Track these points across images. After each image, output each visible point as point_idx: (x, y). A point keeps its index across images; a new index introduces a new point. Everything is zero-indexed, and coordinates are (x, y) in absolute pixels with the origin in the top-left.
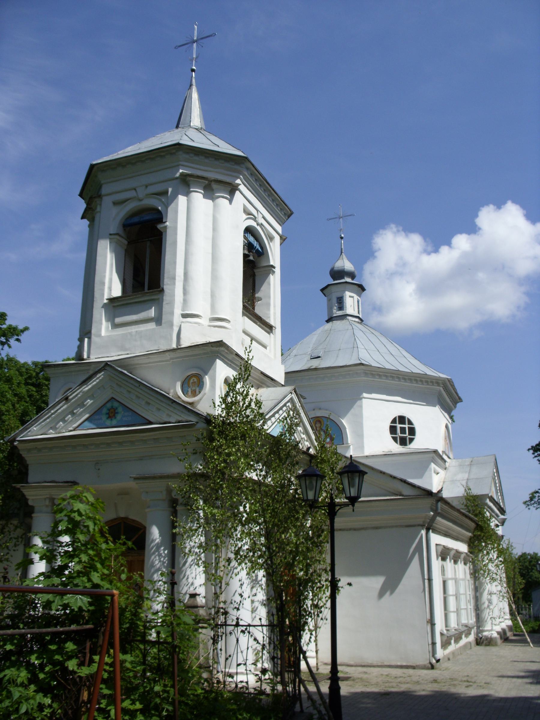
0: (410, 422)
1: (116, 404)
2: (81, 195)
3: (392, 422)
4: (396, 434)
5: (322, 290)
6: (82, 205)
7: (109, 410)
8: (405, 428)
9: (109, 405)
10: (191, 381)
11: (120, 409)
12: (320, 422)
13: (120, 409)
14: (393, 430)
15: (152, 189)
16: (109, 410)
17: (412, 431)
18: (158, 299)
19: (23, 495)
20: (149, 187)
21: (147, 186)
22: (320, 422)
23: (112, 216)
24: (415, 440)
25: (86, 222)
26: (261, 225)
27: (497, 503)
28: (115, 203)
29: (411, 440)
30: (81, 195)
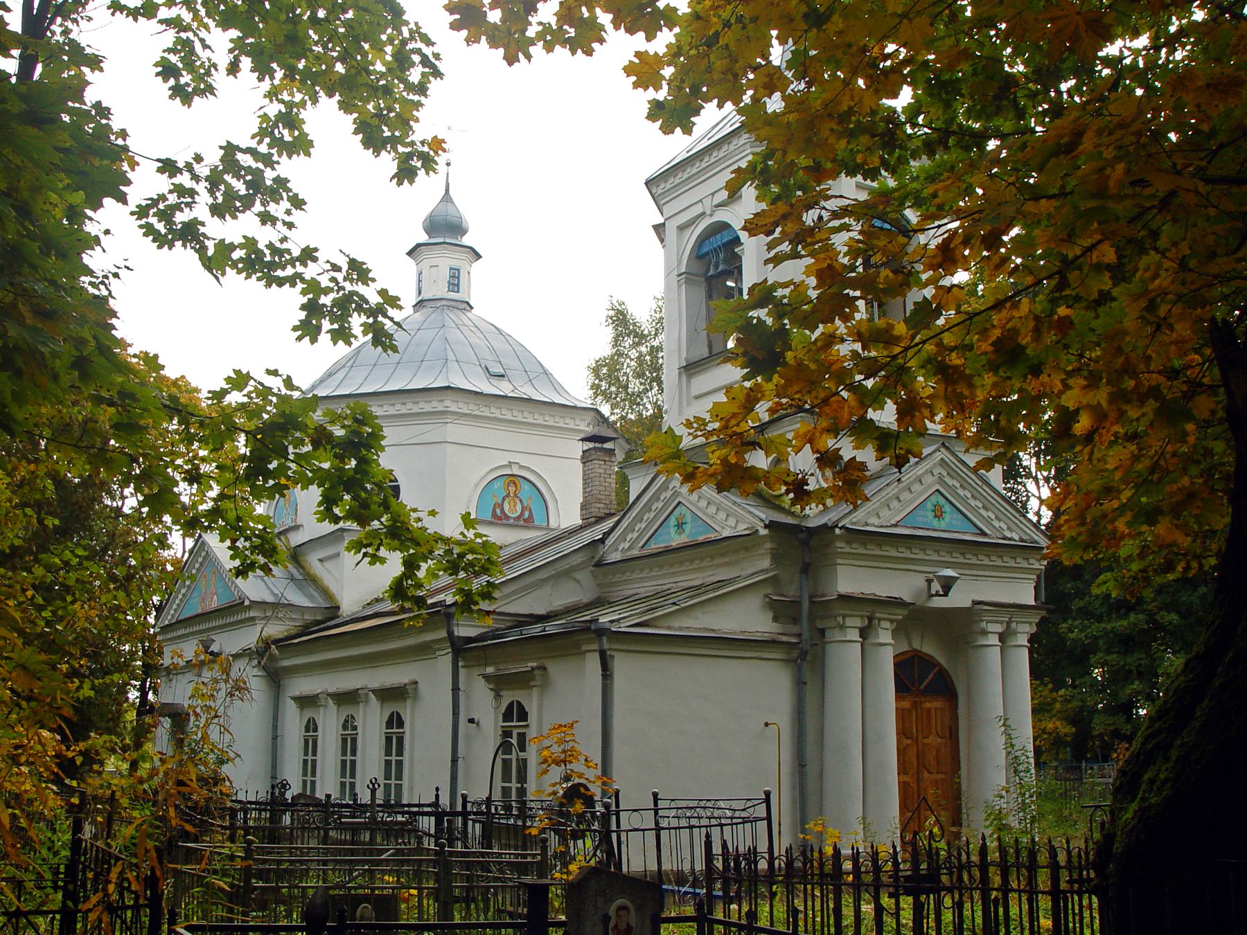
5: (410, 253)
12: (515, 483)
22: (515, 483)
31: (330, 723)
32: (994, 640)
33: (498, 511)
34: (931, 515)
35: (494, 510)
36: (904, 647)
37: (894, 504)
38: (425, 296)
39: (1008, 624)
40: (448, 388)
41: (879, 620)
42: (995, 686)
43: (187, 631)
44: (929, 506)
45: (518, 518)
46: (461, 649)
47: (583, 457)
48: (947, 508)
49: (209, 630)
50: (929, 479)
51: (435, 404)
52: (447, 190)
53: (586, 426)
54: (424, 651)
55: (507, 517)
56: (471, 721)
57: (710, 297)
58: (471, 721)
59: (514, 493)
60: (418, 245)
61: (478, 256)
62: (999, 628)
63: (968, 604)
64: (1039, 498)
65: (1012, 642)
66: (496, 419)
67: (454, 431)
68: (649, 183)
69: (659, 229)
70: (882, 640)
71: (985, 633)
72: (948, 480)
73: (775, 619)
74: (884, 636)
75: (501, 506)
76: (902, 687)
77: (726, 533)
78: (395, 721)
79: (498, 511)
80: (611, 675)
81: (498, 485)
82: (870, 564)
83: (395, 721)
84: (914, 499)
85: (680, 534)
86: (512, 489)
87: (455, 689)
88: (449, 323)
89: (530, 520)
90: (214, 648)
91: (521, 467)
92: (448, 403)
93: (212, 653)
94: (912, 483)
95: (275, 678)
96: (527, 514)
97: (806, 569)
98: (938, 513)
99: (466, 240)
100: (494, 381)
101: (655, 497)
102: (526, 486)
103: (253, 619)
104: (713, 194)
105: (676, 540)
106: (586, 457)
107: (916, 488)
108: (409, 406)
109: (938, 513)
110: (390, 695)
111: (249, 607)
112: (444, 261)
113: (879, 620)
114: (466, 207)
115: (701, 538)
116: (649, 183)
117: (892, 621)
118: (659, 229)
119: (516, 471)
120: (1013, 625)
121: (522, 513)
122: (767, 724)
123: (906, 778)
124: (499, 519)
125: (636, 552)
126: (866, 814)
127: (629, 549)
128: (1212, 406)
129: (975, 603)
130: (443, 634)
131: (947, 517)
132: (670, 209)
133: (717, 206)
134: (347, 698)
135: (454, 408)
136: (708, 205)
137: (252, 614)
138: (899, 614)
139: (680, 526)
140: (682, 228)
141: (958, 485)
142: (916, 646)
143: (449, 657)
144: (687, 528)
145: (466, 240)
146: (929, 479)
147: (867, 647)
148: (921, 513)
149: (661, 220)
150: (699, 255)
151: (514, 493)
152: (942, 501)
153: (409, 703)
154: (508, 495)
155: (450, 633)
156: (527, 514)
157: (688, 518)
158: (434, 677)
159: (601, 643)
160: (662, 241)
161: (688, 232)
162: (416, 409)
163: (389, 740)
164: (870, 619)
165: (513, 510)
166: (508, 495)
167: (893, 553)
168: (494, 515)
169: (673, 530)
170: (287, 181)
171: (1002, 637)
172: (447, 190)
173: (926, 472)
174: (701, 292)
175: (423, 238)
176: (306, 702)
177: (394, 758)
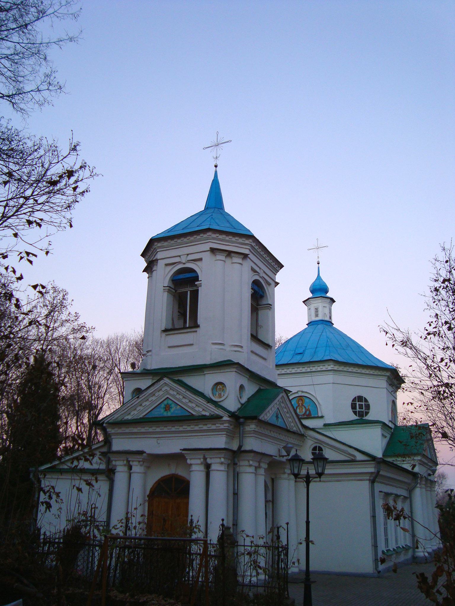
0: (366, 401)
1: (170, 402)
2: (143, 255)
3: (353, 401)
4: (356, 409)
5: (304, 302)
6: (144, 264)
7: (166, 406)
8: (362, 405)
9: (165, 402)
10: (218, 387)
11: (173, 405)
12: (302, 400)
13: (173, 405)
14: (353, 406)
15: (191, 257)
16: (166, 406)
17: (368, 407)
18: (196, 331)
19: (218, 541)
20: (189, 256)
21: (188, 255)
22: (302, 400)
23: (164, 274)
24: (370, 414)
25: (146, 275)
26: (263, 278)
27: (431, 459)
28: (167, 265)
29: (367, 413)
30: (143, 255)
44: (163, 405)
45: (304, 415)
52: (319, 274)
61: (334, 301)
82: (205, 434)
86: (300, 402)
87: (266, 506)
91: (302, 392)
96: (308, 412)
99: (328, 295)
102: (307, 400)
108: (327, 367)
109: (168, 408)
114: (325, 279)
119: (300, 394)
121: (306, 412)
128: (443, 356)
138: (268, 460)
145: (328, 295)
150: (262, 297)
152: (170, 402)
154: (299, 405)
156: (308, 412)
166: (299, 405)
172: (319, 274)
175: (310, 295)
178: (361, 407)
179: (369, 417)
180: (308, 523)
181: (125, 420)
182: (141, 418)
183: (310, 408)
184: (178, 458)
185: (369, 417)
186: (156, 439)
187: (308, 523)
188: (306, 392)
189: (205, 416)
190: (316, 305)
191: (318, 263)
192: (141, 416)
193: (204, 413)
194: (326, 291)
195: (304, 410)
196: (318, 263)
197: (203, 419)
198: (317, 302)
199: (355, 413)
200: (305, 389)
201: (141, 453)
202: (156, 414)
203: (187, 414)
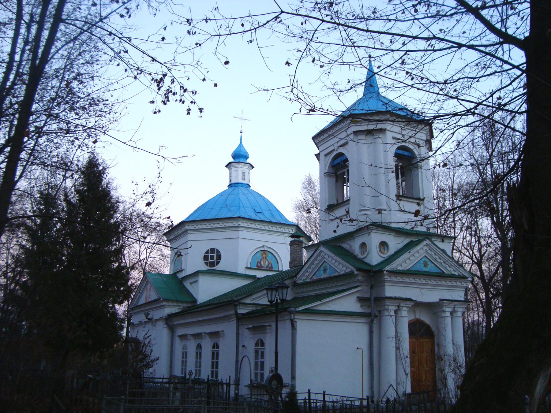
5: (226, 166)
9: (423, 259)
14: (206, 258)
29: (218, 263)
31: (192, 346)
32: (448, 314)
33: (259, 264)
34: (422, 266)
35: (257, 265)
36: (412, 317)
37: (408, 261)
38: (233, 182)
39: (454, 308)
40: (240, 217)
41: (402, 307)
42: (449, 333)
43: (149, 308)
44: (422, 262)
45: (267, 267)
46: (240, 318)
47: (290, 244)
48: (429, 263)
49: (148, 310)
50: (421, 252)
51: (230, 224)
52: (241, 142)
53: (292, 231)
54: (226, 318)
55: (262, 267)
56: (243, 346)
57: (337, 181)
58: (243, 346)
59: (265, 256)
60: (230, 163)
61: (253, 167)
62: (450, 310)
63: (436, 300)
64: (377, 73)
65: (454, 315)
66: (258, 229)
67: (242, 233)
68: (314, 138)
69: (317, 156)
70: (403, 315)
71: (444, 311)
72: (429, 252)
73: (361, 306)
74: (404, 312)
75: (260, 263)
76: (412, 333)
77: (342, 273)
78: (216, 346)
79: (259, 264)
80: (296, 329)
81: (258, 255)
83: (216, 346)
84: (416, 260)
85: (325, 273)
86: (264, 256)
87: (238, 334)
88: (240, 192)
89: (272, 267)
90: (150, 317)
91: (268, 247)
92: (240, 223)
93: (149, 319)
94: (415, 253)
95: (172, 329)
96: (270, 266)
97: (372, 287)
98: (426, 265)
100: (258, 214)
101: (316, 259)
102: (270, 255)
103: (164, 305)
104: (338, 142)
105: (324, 276)
106: (292, 244)
107: (417, 255)
108: (225, 224)
109: (426, 265)
110: (215, 335)
111: (162, 301)
112: (242, 168)
113: (402, 307)
114: (248, 148)
115: (333, 275)
116: (314, 138)
117: (407, 307)
118: (317, 156)
119: (266, 249)
120: (456, 309)
121: (268, 265)
122: (358, 348)
123: (413, 369)
124: (259, 268)
125: (308, 280)
126: (397, 379)
127: (306, 279)
129: (441, 300)
130: (233, 312)
131: (429, 266)
132: (322, 148)
133: (339, 147)
134: (197, 336)
135: (242, 225)
136: (336, 146)
137: (164, 303)
138: (411, 304)
139: (325, 270)
140: (326, 155)
141: (433, 254)
142: (418, 317)
143: (235, 321)
144: (328, 271)
146: (421, 252)
147: (397, 318)
148: (419, 265)
149: (318, 152)
151: (265, 256)
152: (427, 260)
153: (221, 339)
154: (263, 258)
155: (236, 312)
156: (270, 266)
157: (328, 267)
158: (229, 329)
159: (291, 317)
160: (319, 160)
161: (329, 156)
162: (209, 227)
163: (213, 353)
164: (399, 306)
165: (264, 264)
167: (407, 280)
168: (257, 266)
169: (322, 272)
170: (396, 195)
171: (451, 313)
172: (241, 142)
173: (420, 249)
174: (333, 180)
175: (232, 160)
176: (183, 337)
177: (215, 360)
178: (212, 257)
179: (221, 267)
180: (276, 353)
181: (398, 270)
182: (407, 270)
183: (272, 262)
184: (434, 308)
185: (221, 267)
186: (419, 289)
187: (276, 353)
188: (270, 248)
189: (455, 275)
190: (244, 169)
191: (241, 132)
192: (408, 268)
193: (453, 273)
194: (247, 157)
195: (267, 263)
196: (241, 132)
197: (452, 277)
198: (245, 167)
199: (207, 264)
200: (269, 245)
201: (410, 300)
202: (417, 268)
203: (440, 271)
